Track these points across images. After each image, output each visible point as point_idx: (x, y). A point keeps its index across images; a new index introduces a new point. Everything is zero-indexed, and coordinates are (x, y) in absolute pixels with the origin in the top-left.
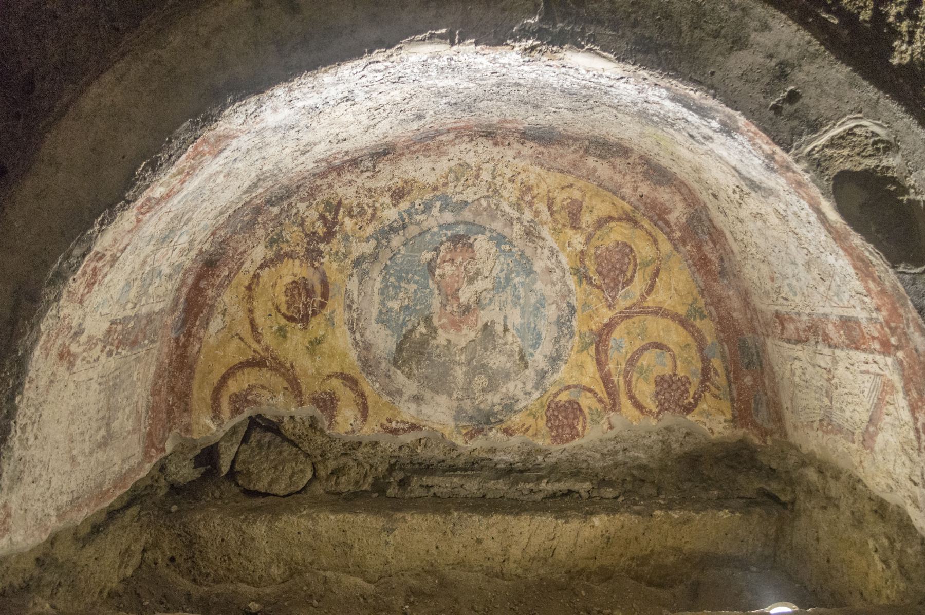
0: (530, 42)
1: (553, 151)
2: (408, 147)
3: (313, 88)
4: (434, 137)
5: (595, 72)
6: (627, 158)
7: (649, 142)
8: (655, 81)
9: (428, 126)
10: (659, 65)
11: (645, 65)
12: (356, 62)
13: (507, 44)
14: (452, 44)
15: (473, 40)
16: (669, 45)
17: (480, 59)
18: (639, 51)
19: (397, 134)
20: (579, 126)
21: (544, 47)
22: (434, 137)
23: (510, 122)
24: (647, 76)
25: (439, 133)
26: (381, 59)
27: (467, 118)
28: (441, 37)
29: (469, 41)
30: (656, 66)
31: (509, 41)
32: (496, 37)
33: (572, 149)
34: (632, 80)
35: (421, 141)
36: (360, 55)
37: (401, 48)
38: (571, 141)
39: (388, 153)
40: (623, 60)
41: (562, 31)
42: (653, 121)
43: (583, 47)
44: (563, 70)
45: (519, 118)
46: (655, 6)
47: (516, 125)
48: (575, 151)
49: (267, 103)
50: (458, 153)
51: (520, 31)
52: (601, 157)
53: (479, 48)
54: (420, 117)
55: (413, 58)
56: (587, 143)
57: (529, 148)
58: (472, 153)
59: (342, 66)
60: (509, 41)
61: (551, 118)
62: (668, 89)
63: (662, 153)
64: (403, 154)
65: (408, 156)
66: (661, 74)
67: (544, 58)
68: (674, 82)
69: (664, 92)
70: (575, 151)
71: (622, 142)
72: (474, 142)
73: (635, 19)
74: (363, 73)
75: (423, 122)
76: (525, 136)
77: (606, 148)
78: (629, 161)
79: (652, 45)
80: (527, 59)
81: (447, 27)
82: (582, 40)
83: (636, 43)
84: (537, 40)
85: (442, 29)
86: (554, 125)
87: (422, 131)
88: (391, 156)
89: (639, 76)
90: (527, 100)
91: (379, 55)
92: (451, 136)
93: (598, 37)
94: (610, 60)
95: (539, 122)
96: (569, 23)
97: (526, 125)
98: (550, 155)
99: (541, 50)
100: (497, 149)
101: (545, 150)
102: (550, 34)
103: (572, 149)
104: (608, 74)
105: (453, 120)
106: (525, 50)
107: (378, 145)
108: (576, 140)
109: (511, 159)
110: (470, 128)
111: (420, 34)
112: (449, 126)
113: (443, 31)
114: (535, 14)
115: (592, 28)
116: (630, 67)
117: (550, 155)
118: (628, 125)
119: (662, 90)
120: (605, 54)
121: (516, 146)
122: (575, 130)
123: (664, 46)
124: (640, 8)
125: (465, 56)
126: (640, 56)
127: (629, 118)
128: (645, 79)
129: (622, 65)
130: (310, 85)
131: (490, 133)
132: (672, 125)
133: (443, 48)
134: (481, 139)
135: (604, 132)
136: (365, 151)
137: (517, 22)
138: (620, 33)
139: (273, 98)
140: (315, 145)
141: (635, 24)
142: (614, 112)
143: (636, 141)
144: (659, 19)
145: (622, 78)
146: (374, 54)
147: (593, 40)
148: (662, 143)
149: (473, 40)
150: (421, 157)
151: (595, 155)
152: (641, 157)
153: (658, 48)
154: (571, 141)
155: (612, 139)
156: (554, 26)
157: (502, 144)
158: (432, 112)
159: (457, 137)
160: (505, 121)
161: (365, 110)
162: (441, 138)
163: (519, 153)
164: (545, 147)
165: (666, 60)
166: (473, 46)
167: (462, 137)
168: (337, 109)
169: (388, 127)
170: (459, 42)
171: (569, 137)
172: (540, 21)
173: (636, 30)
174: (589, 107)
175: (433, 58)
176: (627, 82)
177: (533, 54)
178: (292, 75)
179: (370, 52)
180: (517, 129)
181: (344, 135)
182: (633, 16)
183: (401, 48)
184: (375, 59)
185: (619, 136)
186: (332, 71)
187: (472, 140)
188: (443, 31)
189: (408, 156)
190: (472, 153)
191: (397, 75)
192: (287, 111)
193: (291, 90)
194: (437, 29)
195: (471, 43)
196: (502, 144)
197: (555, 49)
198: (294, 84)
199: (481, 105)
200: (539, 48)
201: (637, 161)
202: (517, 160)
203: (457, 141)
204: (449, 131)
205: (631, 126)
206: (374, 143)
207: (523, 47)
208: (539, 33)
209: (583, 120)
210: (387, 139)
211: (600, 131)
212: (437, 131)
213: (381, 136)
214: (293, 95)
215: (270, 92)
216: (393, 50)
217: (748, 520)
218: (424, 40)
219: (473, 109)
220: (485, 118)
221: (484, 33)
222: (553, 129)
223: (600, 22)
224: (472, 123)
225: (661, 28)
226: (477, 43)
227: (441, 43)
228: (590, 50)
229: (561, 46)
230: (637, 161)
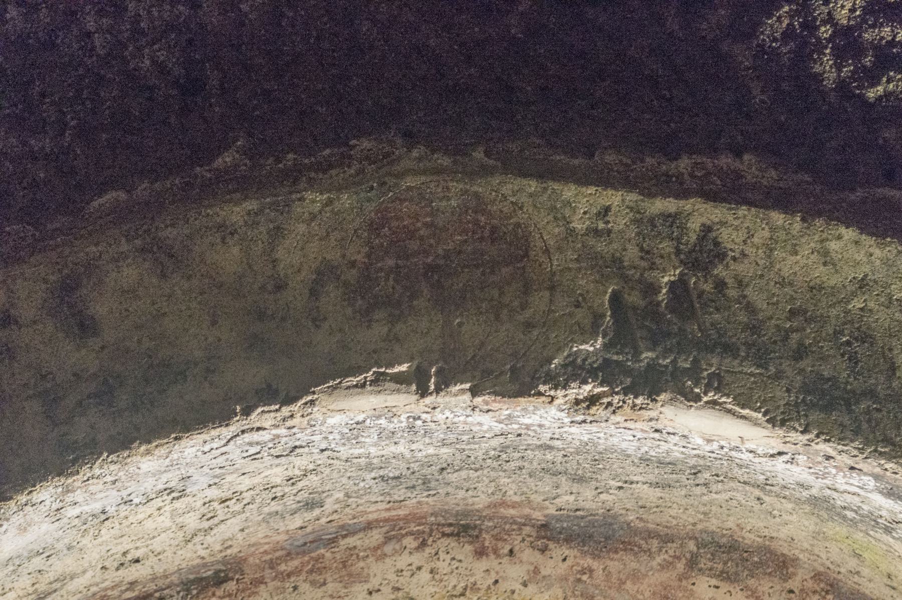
0: (588, 388)
1: (614, 566)
2: (272, 564)
3: (114, 482)
4: (334, 541)
5: (723, 443)
6: (786, 578)
7: (834, 548)
8: (850, 462)
9: (324, 520)
10: (857, 432)
11: (826, 433)
12: (214, 433)
13: (540, 394)
14: (423, 392)
15: (468, 386)
16: (871, 393)
17: (477, 417)
18: (813, 405)
19: (253, 540)
20: (673, 512)
21: (616, 399)
22: (334, 541)
23: (514, 505)
24: (833, 453)
25: (347, 531)
26: (266, 425)
27: (416, 501)
28: (399, 379)
29: (459, 387)
30: (849, 434)
31: (542, 388)
32: (518, 378)
33: (659, 559)
34: (801, 459)
35: (303, 549)
36: (224, 419)
37: (312, 402)
38: (655, 543)
39: (226, 579)
40: (783, 423)
41: (652, 366)
42: (844, 517)
43: (697, 398)
44: (657, 435)
45: (537, 499)
46: (837, 317)
47: (527, 511)
48: (666, 566)
49: (14, 519)
50: (392, 577)
51: (565, 366)
52: (725, 576)
53: (478, 400)
54: (309, 505)
55: (335, 420)
56: (692, 546)
57: (559, 561)
58: (424, 575)
59: (184, 442)
60: (542, 388)
61: (610, 498)
62: (876, 477)
63: (865, 571)
64: (261, 581)
65: (272, 585)
66: (861, 451)
67: (618, 418)
68: (889, 466)
69: (871, 483)
70: (666, 566)
71: (774, 545)
72: (428, 550)
73: (801, 344)
74: (224, 449)
75: (317, 512)
76: (547, 533)
77: (735, 556)
78: (790, 585)
79: (837, 393)
80: (580, 418)
81: (411, 359)
82: (696, 385)
83: (806, 389)
84: (601, 384)
85: (400, 364)
86: (617, 509)
87: (309, 529)
88: (231, 586)
89: (817, 452)
90: (559, 468)
91: (265, 417)
92: (376, 536)
93: (728, 378)
94: (756, 424)
95: (582, 504)
96: (666, 352)
97: (552, 511)
98: (608, 575)
99: (610, 404)
100: (484, 564)
101: (595, 564)
102: (628, 372)
103: (659, 559)
104: (752, 446)
105: (384, 506)
106: (577, 402)
107: (205, 565)
108: (666, 539)
109: (518, 587)
110: (419, 519)
111: (354, 376)
112: (371, 517)
113: (404, 368)
114: (594, 334)
115: (715, 361)
116: (794, 436)
117: (608, 575)
118: (785, 517)
119: (866, 478)
120: (745, 412)
121: (528, 555)
122: (664, 519)
123: (864, 394)
124: (808, 321)
125: (448, 413)
126: (815, 416)
127: (790, 506)
128: (828, 458)
129: (781, 432)
130: (109, 479)
131: (466, 528)
132: (888, 530)
133: (404, 402)
134: (445, 541)
135: (731, 524)
136: (175, 579)
137: (559, 350)
138: (773, 370)
139: (28, 508)
140: (72, 578)
141: (800, 353)
142: (757, 492)
143: (806, 545)
144: (848, 343)
145: (780, 454)
146: (254, 416)
147: (717, 383)
148: (865, 555)
149: (468, 386)
150: (305, 587)
151: (711, 572)
152: (817, 576)
153: (849, 400)
154: (655, 543)
155: (750, 538)
156: (637, 353)
157: (496, 551)
158: (341, 495)
159: (388, 539)
160: (503, 504)
161: (199, 504)
162: (351, 541)
163: (536, 571)
164: (595, 557)
165: (869, 421)
166: (467, 397)
167: (399, 538)
168: (141, 509)
169: (238, 528)
170: (438, 390)
171: (650, 535)
172: (605, 346)
173: (802, 364)
174: (702, 481)
175: (379, 417)
176: (792, 461)
177: (593, 410)
178: (74, 462)
179: (247, 412)
180: (528, 518)
181: (138, 554)
182: (795, 336)
183: (312, 402)
184: (258, 425)
185: (766, 532)
186: (163, 451)
187: (423, 544)
188: (404, 368)
189: (272, 585)
190: (424, 575)
191: (291, 444)
192: (46, 527)
193: (68, 490)
194: (391, 365)
195: (463, 391)
196: (496, 551)
197: (639, 401)
198: (76, 481)
199: (453, 477)
200: (605, 400)
201: (810, 584)
202: (532, 588)
203: (388, 549)
204: (369, 526)
205: (794, 518)
206: (198, 561)
207: (571, 397)
208: (603, 370)
209: (684, 502)
210: (229, 552)
211: (721, 522)
212: (342, 527)
213: (218, 547)
214: (69, 498)
215: (23, 498)
216: (295, 407)
217: (733, 539)
218: (363, 386)
219: (433, 484)
220: (458, 499)
221: (487, 373)
222: (615, 517)
223: (729, 349)
224: (425, 509)
225: (853, 359)
226: (475, 392)
227: (398, 391)
228: (713, 403)
229: (652, 395)
230: (810, 584)
